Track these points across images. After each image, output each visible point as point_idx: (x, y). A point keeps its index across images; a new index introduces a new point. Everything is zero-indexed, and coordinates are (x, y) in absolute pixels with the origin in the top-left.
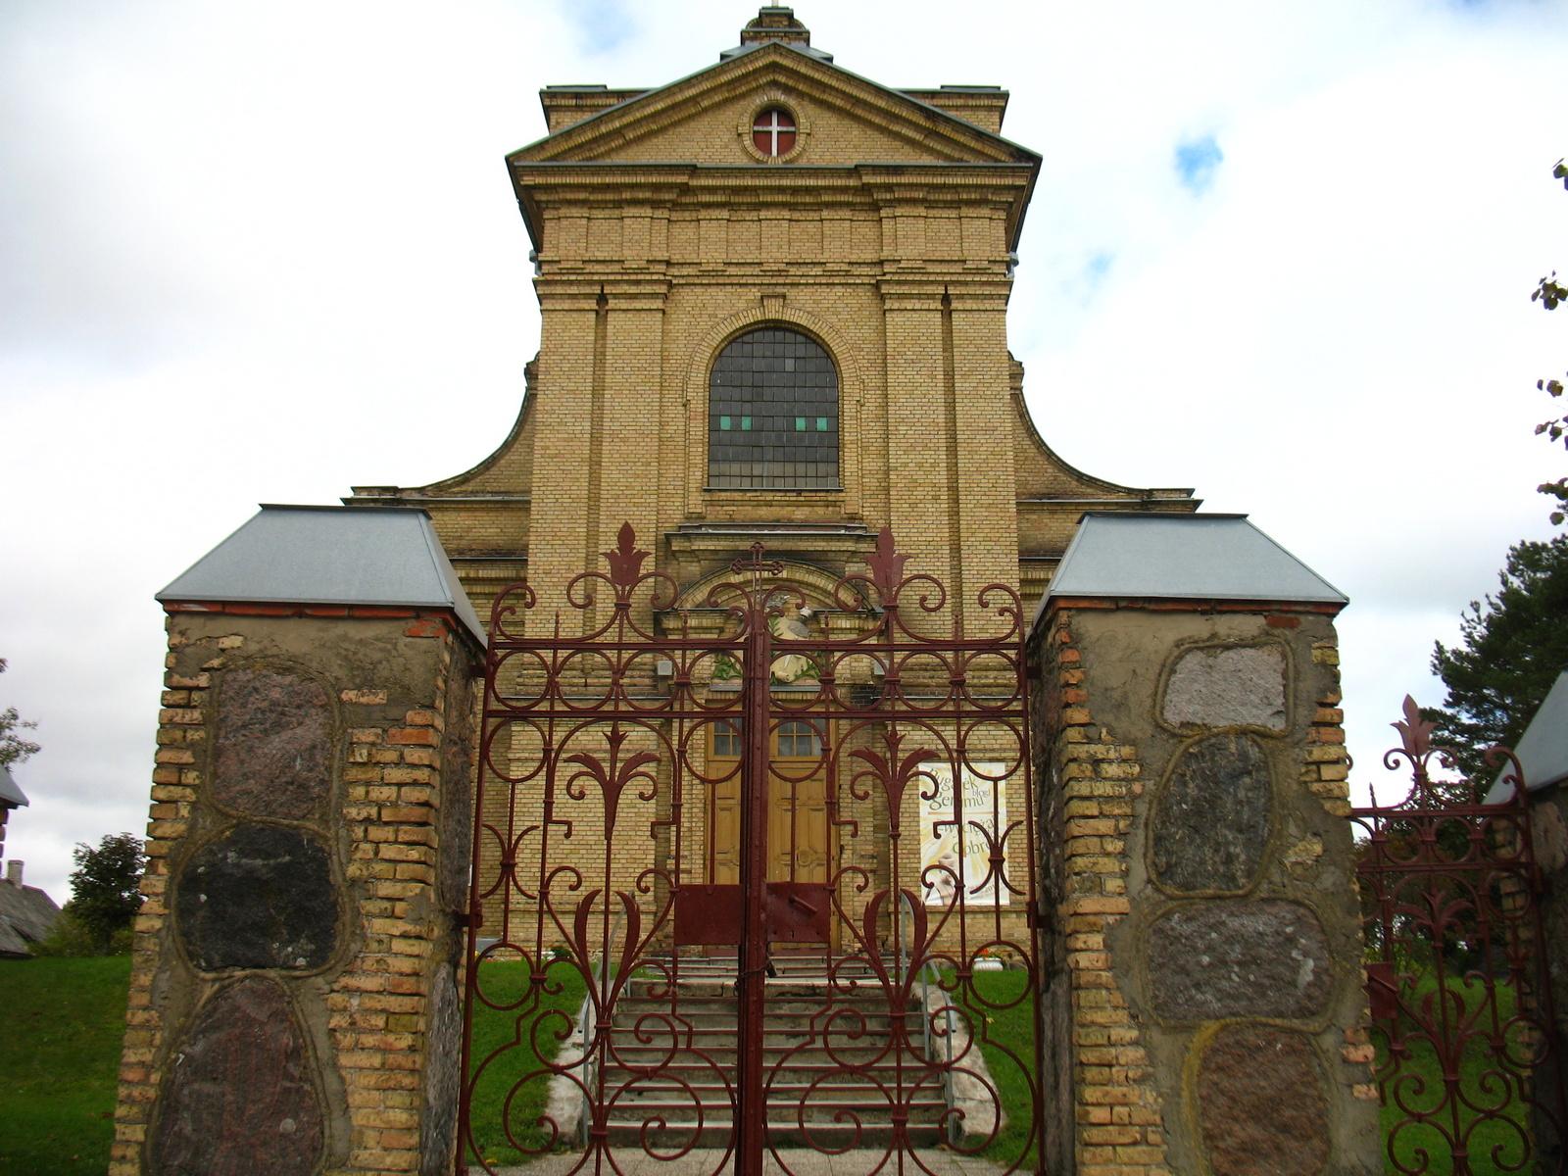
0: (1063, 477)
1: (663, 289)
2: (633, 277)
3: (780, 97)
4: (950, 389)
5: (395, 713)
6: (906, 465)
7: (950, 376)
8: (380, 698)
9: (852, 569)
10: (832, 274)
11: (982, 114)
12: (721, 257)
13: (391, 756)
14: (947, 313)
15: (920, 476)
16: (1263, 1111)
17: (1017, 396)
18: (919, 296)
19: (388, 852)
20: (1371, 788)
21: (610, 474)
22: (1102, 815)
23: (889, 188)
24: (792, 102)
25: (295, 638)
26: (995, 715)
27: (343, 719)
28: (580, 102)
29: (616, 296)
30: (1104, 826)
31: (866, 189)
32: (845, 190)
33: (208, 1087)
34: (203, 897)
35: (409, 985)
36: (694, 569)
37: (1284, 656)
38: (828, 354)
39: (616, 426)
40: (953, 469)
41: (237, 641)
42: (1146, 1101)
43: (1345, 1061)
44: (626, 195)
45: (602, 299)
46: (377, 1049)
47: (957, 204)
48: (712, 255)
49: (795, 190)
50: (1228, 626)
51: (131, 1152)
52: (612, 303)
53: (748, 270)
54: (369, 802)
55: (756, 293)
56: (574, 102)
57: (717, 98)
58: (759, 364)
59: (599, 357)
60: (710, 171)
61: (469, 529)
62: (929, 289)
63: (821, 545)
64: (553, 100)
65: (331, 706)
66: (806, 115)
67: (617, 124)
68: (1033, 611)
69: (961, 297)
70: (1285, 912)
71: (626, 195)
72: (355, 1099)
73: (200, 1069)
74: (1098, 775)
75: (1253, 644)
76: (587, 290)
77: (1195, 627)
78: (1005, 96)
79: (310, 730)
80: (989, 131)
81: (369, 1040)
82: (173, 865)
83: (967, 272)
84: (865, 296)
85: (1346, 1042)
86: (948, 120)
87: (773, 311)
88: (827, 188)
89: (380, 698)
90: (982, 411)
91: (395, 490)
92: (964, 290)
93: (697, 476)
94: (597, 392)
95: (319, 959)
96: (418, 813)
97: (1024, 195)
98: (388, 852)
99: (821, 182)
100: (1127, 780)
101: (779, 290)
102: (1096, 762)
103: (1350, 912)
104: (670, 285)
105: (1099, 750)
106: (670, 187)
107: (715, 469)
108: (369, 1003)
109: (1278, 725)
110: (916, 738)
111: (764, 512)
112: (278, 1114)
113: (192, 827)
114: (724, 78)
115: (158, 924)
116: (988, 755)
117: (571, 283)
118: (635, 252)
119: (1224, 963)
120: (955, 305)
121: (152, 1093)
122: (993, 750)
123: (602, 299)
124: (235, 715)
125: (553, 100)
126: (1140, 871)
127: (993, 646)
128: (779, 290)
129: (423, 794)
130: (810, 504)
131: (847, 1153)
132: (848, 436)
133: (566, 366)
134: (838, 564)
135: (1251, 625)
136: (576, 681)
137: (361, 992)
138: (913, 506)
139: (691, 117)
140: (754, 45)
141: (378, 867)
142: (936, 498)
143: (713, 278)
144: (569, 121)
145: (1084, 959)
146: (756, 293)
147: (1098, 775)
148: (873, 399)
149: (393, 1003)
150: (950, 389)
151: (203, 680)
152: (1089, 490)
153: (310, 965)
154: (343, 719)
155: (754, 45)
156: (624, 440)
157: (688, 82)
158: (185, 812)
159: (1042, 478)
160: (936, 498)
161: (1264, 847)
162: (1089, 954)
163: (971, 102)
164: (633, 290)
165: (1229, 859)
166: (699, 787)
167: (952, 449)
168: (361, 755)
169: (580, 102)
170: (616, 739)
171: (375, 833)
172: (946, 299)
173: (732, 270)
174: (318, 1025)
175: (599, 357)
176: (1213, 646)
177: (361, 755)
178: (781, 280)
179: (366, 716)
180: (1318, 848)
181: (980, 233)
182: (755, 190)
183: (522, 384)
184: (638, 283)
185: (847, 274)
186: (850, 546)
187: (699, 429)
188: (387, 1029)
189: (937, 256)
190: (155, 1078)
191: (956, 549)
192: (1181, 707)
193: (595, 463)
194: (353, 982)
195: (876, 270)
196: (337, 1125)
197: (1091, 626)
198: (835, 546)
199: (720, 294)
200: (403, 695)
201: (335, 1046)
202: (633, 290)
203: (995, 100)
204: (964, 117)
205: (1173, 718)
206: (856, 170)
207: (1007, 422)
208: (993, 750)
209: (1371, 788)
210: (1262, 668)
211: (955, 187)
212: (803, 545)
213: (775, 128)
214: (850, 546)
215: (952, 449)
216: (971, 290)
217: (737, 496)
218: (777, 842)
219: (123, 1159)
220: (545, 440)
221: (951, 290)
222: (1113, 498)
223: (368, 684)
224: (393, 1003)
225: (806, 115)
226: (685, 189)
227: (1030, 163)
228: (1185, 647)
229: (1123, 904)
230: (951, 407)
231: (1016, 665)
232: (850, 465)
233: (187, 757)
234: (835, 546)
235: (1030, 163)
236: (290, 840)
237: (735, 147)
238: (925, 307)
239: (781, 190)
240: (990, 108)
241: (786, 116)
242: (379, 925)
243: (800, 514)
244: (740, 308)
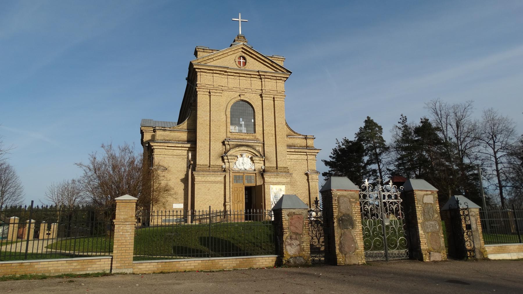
0: (291, 132)
2: (216, 89)
3: (244, 55)
5: (356, 201)
6: (267, 129)
8: (354, 200)
11: (280, 62)
13: (356, 206)
15: (269, 132)
22: (419, 212)
23: (264, 75)
28: (204, 51)
30: (419, 213)
34: (341, 222)
37: (433, 196)
39: (213, 119)
41: (339, 194)
43: (441, 236)
44: (214, 72)
46: (359, 237)
51: (338, 249)
53: (237, 89)
54: (355, 211)
56: (203, 51)
57: (231, 53)
60: (231, 69)
61: (180, 136)
62: (271, 96)
63: (252, 144)
69: (276, 98)
71: (214, 72)
72: (358, 242)
75: (430, 194)
76: (207, 90)
81: (358, 236)
83: (277, 93)
95: (353, 228)
100: (421, 209)
102: (418, 207)
104: (223, 91)
108: (358, 232)
109: (433, 203)
111: (241, 137)
113: (338, 214)
115: (336, 225)
116: (283, 184)
117: (204, 89)
118: (216, 84)
119: (430, 227)
121: (339, 243)
122: (283, 183)
126: (423, 218)
133: (203, 106)
134: (255, 148)
136: (207, 168)
137: (357, 231)
138: (268, 137)
142: (272, 136)
143: (230, 90)
147: (418, 208)
151: (337, 198)
152: (296, 135)
153: (352, 229)
156: (215, 122)
158: (337, 213)
160: (272, 136)
163: (278, 59)
164: (216, 91)
166: (94, 172)
169: (204, 51)
171: (356, 215)
173: (234, 89)
176: (427, 195)
177: (353, 206)
178: (243, 92)
179: (353, 202)
180: (437, 215)
184: (217, 90)
186: (257, 144)
188: (360, 235)
189: (272, 89)
190: (339, 241)
194: (356, 230)
198: (255, 144)
201: (355, 237)
202: (216, 91)
205: (424, 202)
208: (283, 183)
211: (276, 76)
219: (337, 250)
221: (275, 96)
223: (354, 199)
225: (248, 58)
226: (226, 72)
233: (336, 207)
234: (255, 144)
237: (235, 64)
238: (270, 99)
241: (244, 58)
242: (358, 224)
243: (248, 137)
244: (234, 97)
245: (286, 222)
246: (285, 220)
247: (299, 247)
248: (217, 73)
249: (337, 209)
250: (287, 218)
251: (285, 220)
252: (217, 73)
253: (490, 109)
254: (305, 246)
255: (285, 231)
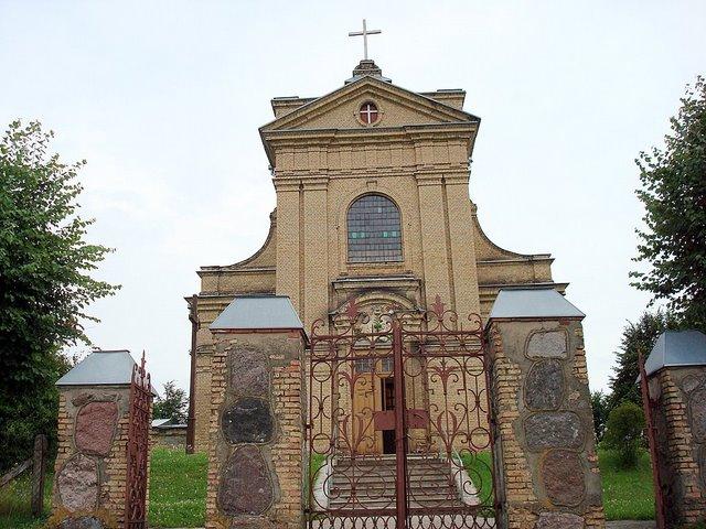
4: (447, 217)
7: (446, 211)
8: (282, 357)
9: (409, 294)
13: (286, 375)
14: (444, 186)
16: (564, 477)
17: (475, 218)
18: (432, 180)
19: (287, 405)
20: (98, 321)
21: (309, 258)
23: (418, 135)
24: (376, 101)
25: (254, 340)
26: (474, 355)
27: (270, 365)
29: (307, 185)
30: (510, 390)
31: (408, 135)
32: (399, 136)
33: (236, 480)
35: (296, 446)
36: (345, 296)
38: (387, 198)
40: (449, 250)
42: (527, 475)
45: (301, 186)
47: (446, 140)
48: (346, 166)
49: (379, 138)
50: (547, 325)
52: (305, 188)
55: (364, 181)
58: (367, 210)
59: (301, 210)
62: (436, 176)
63: (396, 284)
64: (277, 104)
65: (267, 360)
66: (380, 104)
67: (304, 113)
68: (485, 322)
70: (568, 414)
72: (281, 482)
73: (233, 475)
74: (507, 374)
77: (537, 326)
78: (464, 93)
79: (261, 368)
80: (458, 108)
82: (220, 412)
84: (410, 180)
85: (589, 455)
86: (441, 105)
87: (372, 188)
89: (282, 357)
90: (460, 226)
91: (219, 267)
92: (450, 176)
93: (344, 258)
94: (301, 224)
96: (296, 393)
97: (474, 134)
98: (287, 405)
99: (390, 134)
101: (374, 179)
102: (507, 370)
103: (589, 415)
104: (329, 179)
105: (508, 366)
106: (327, 138)
107: (351, 254)
111: (372, 271)
112: (258, 488)
114: (347, 92)
123: (301, 186)
124: (237, 364)
125: (277, 104)
126: (522, 403)
127: (473, 333)
128: (374, 179)
129: (295, 387)
130: (390, 267)
132: (405, 239)
135: (555, 324)
140: (359, 77)
141: (284, 410)
144: (284, 112)
145: (505, 431)
146: (364, 181)
148: (415, 223)
149: (292, 452)
150: (447, 217)
154: (270, 365)
155: (359, 77)
157: (329, 96)
159: (487, 252)
161: (562, 395)
162: (507, 429)
164: (314, 182)
165: (550, 399)
167: (449, 242)
168: (277, 375)
170: (443, 363)
173: (354, 172)
174: (269, 460)
175: (301, 210)
177: (277, 375)
181: (455, 152)
182: (362, 138)
183: (268, 223)
186: (408, 284)
187: (344, 238)
191: (452, 284)
192: (533, 351)
193: (302, 254)
195: (414, 169)
196: (277, 490)
197: (503, 327)
198: (401, 284)
199: (350, 182)
200: (289, 356)
202: (314, 182)
203: (460, 95)
204: (447, 103)
206: (404, 128)
207: (472, 229)
209: (98, 321)
210: (558, 338)
212: (388, 285)
213: (369, 111)
214: (408, 284)
215: (449, 242)
216: (454, 175)
217: (361, 265)
218: (408, 402)
220: (281, 245)
222: (517, 259)
224: (292, 452)
225: (380, 104)
226: (333, 139)
227: (476, 121)
228: (533, 333)
229: (517, 414)
230: (447, 224)
231: (481, 338)
232: (406, 251)
233: (222, 378)
234: (401, 284)
235: (476, 121)
236: (257, 403)
239: (373, 137)
240: (459, 99)
241: (373, 106)
243: (387, 272)
245: (67, 421)
246: (65, 415)
247: (94, 490)
248: (316, 145)
249: (224, 384)
250: (73, 411)
251: (65, 415)
252: (316, 145)
253: (45, 129)
254: (113, 489)
255: (61, 444)
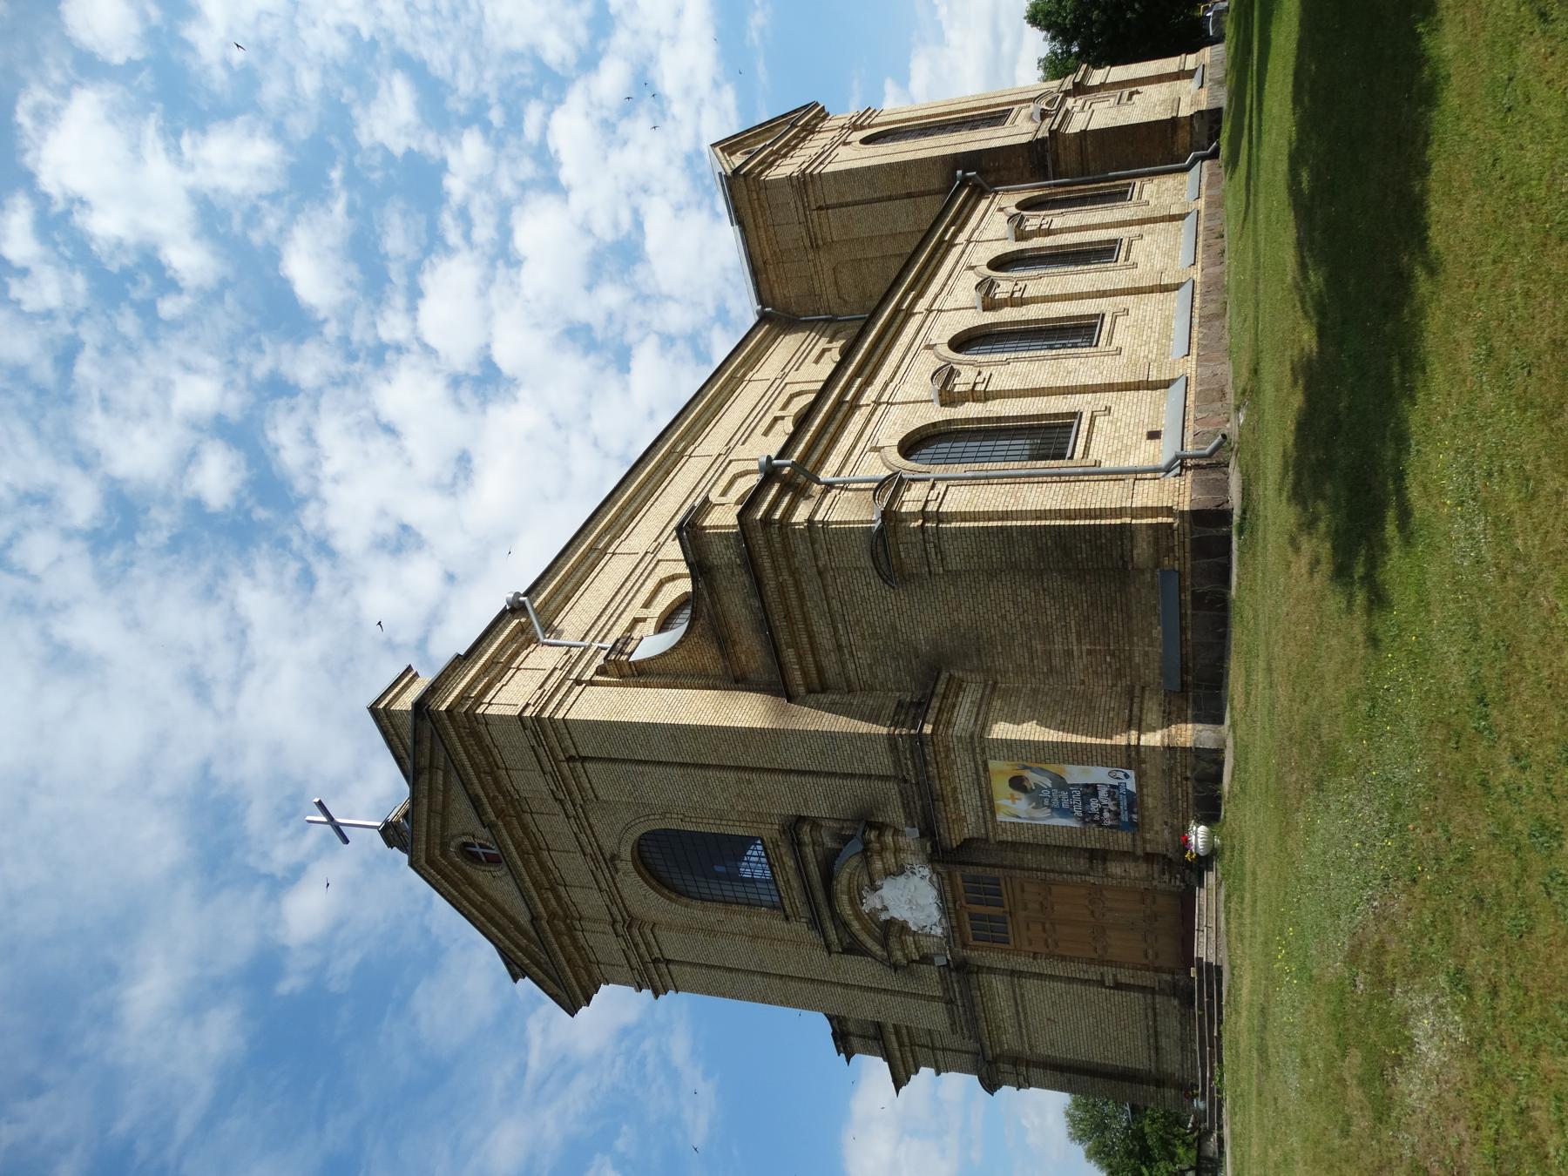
1: (635, 932)
10: (581, 827)
12: (597, 894)
23: (492, 800)
31: (500, 813)
52: (657, 954)
64: (515, 979)
88: (512, 836)
92: (558, 750)
110: (973, 820)
120: (822, 203)
122: (977, 769)
131: (1289, 216)
139: (494, 903)
172: (820, 208)
185: (577, 817)
244: (633, 886)
